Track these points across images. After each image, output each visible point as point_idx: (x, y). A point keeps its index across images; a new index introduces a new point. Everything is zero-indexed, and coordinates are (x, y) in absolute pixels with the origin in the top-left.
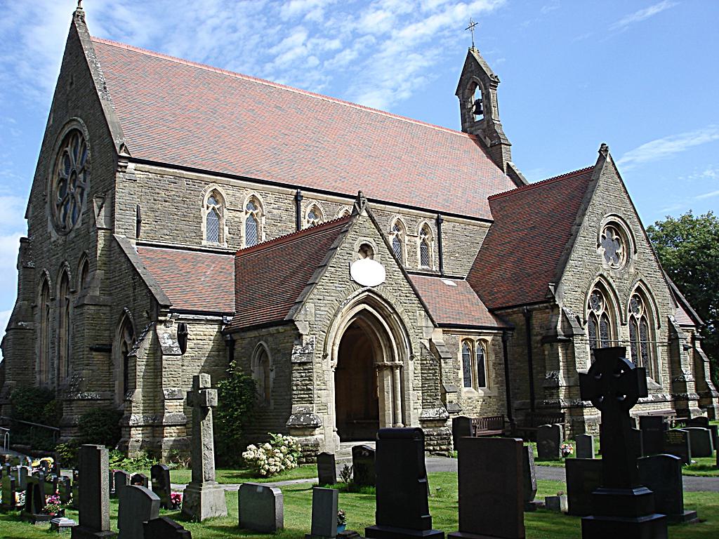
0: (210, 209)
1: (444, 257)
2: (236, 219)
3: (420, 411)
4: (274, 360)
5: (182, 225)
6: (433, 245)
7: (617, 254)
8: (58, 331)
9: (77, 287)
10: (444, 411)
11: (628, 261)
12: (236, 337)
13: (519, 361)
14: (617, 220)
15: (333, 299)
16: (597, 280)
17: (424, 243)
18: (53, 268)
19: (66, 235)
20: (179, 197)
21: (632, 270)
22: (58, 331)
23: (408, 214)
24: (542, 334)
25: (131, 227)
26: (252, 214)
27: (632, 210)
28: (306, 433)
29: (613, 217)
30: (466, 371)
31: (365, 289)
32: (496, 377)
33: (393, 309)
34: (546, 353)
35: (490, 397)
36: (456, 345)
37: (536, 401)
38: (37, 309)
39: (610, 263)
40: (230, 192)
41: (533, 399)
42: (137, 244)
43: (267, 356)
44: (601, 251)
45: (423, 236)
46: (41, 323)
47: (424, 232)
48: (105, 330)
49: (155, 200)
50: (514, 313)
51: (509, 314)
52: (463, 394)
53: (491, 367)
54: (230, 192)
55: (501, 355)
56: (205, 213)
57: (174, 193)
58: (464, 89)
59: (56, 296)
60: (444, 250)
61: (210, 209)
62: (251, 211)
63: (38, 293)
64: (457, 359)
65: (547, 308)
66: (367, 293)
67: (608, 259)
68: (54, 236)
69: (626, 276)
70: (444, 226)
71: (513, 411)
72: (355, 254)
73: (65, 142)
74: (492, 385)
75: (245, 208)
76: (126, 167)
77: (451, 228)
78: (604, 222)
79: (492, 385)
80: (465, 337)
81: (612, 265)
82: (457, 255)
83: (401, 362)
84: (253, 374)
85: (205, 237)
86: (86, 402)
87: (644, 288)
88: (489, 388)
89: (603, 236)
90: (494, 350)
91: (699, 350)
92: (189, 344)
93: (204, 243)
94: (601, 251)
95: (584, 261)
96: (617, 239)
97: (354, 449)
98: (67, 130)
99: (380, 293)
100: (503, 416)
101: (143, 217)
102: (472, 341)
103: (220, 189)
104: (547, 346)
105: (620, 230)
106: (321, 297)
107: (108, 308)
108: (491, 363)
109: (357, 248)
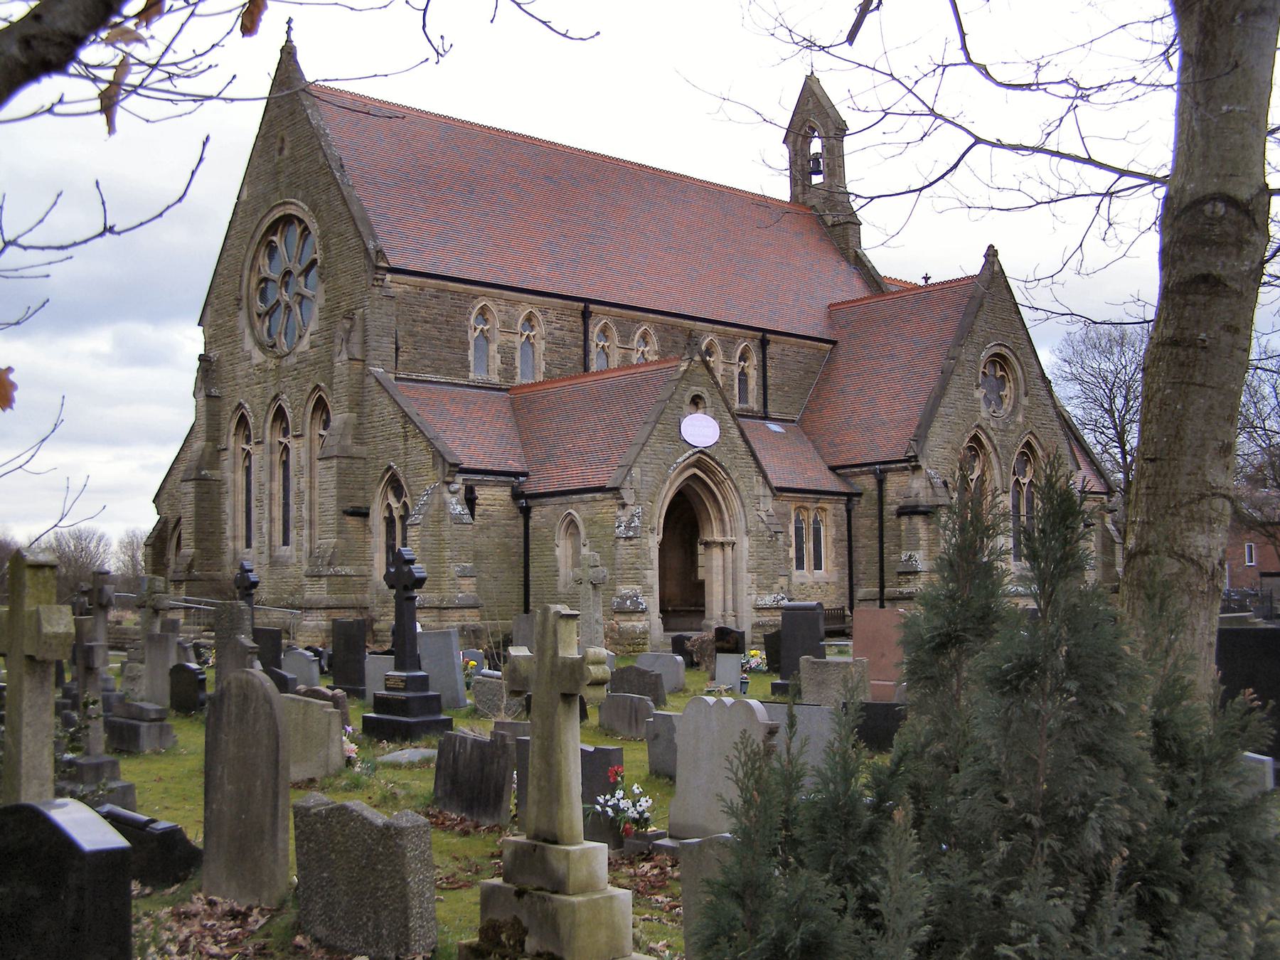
0: (478, 331)
1: (769, 392)
2: (510, 344)
3: (754, 597)
4: (588, 534)
5: (445, 353)
6: (753, 375)
7: (1000, 397)
8: (267, 485)
9: (303, 429)
10: (783, 598)
11: (1014, 407)
12: (531, 503)
13: (867, 537)
14: (1004, 351)
15: (661, 462)
16: (973, 433)
17: (743, 375)
18: (256, 401)
19: (280, 357)
20: (442, 315)
21: (1020, 419)
22: (267, 485)
23: (725, 334)
24: (898, 503)
25: (389, 358)
26: (528, 337)
27: (1025, 337)
28: (633, 618)
29: (998, 348)
30: (799, 550)
31: (697, 450)
32: (836, 557)
33: (728, 474)
34: (903, 527)
35: (827, 583)
36: (787, 515)
37: (886, 590)
38: (227, 453)
39: (991, 410)
40: (503, 308)
41: (882, 587)
42: (397, 379)
43: (577, 527)
44: (979, 394)
45: (742, 363)
46: (234, 472)
47: (743, 358)
48: (360, 489)
49: (414, 321)
50: (863, 473)
51: (856, 474)
52: (794, 579)
53: (830, 545)
54: (503, 308)
55: (844, 529)
56: (472, 335)
57: (436, 311)
58: (797, 134)
59: (264, 438)
60: (770, 381)
61: (478, 331)
62: (527, 333)
63: (229, 431)
64: (788, 532)
65: (906, 469)
66: (698, 455)
67: (988, 403)
68: (258, 357)
69: (1011, 427)
70: (772, 349)
71: (856, 601)
72: (686, 408)
73: (273, 229)
74: (830, 568)
75: (519, 328)
76: (383, 280)
77: (779, 352)
78: (984, 355)
79: (830, 568)
80: (799, 504)
81: (994, 412)
82: (786, 389)
83: (734, 538)
84: (557, 549)
85: (472, 368)
86: (340, 579)
87: (1034, 442)
88: (826, 571)
89: (984, 373)
90: (835, 522)
91: (1111, 527)
92: (478, 510)
93: (471, 376)
94: (979, 394)
95: (957, 408)
96: (1002, 376)
97: (427, 690)
98: (277, 214)
99: (712, 455)
100: (843, 609)
101: (400, 343)
102: (807, 509)
103: (490, 304)
104: (905, 520)
105: (1007, 364)
106: (648, 461)
107: (363, 462)
108: (830, 540)
109: (687, 400)
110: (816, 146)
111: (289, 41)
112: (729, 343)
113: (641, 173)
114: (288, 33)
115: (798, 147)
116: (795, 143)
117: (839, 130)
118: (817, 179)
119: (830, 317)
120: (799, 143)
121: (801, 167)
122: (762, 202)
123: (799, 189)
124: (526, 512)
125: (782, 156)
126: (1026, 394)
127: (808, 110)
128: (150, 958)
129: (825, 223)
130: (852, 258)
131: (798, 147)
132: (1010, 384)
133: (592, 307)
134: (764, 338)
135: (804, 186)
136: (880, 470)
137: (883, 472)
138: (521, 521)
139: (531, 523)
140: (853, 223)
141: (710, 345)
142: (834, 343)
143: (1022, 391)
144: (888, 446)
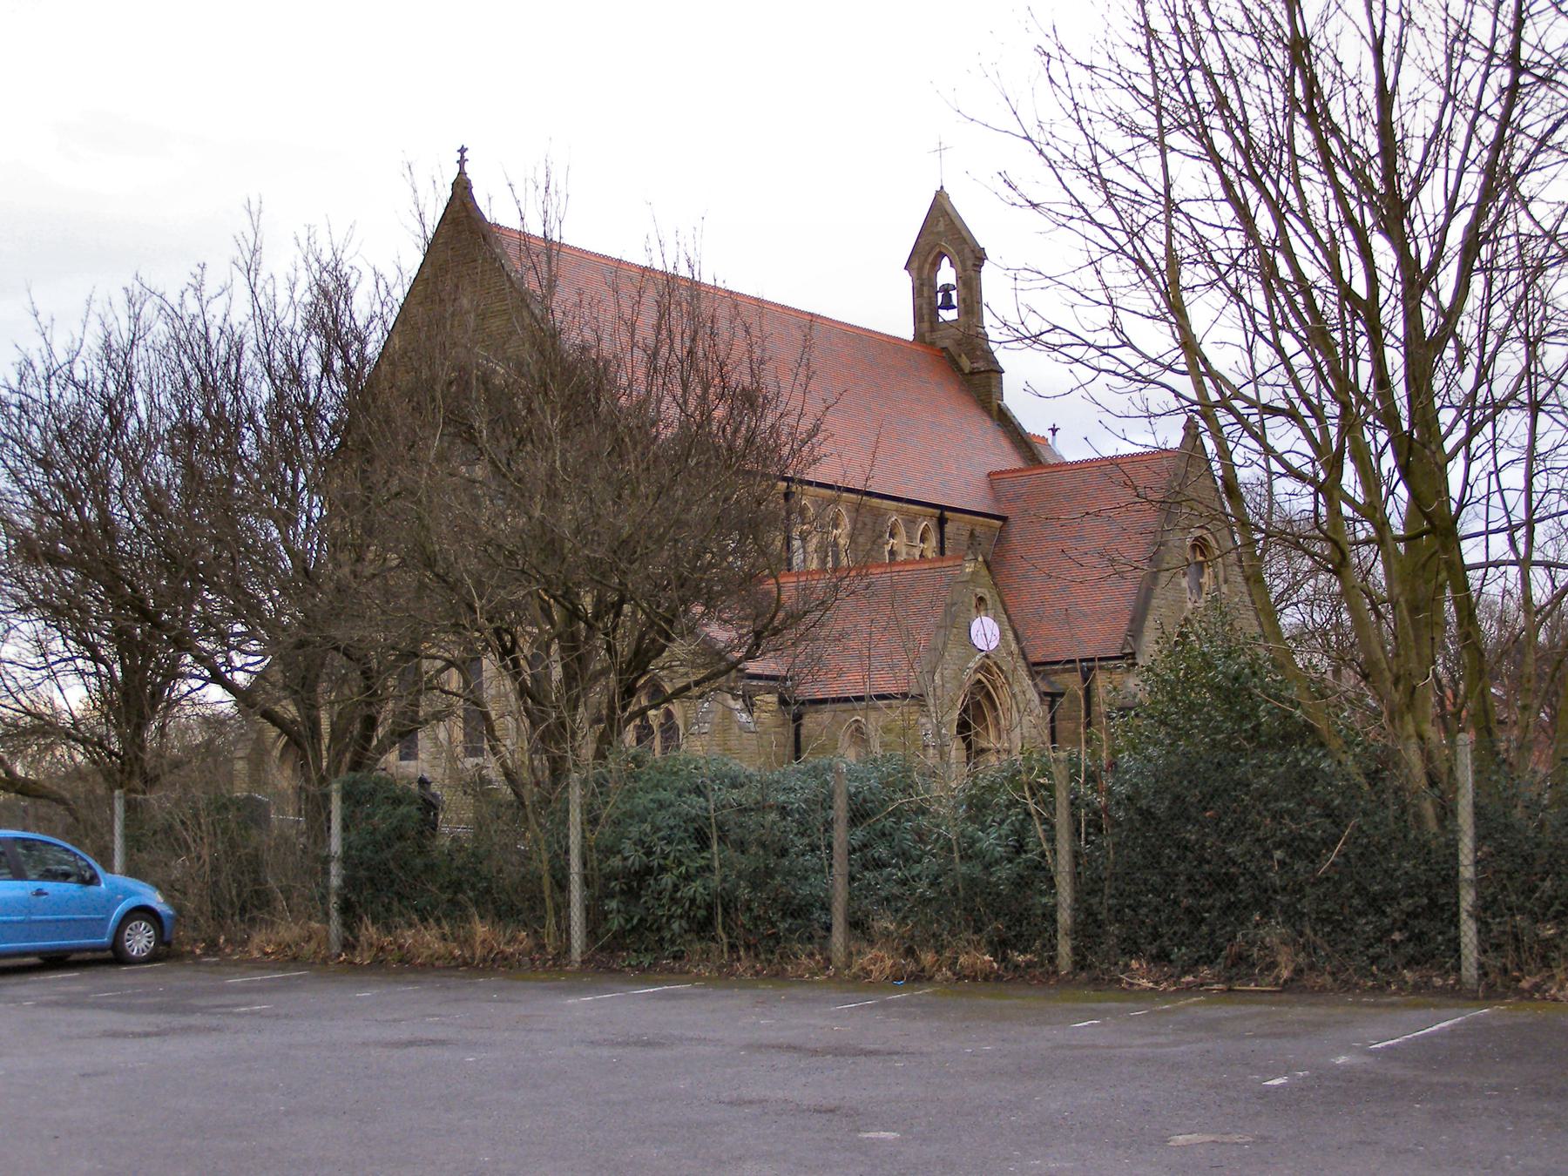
23: (907, 512)
50: (1065, 671)
51: (1056, 672)
58: (922, 261)
70: (949, 528)
110: (947, 274)
111: (462, 173)
112: (911, 521)
113: (784, 316)
114: (462, 162)
115: (925, 276)
116: (920, 269)
117: (972, 258)
118: (949, 315)
119: (992, 488)
120: (926, 271)
121: (926, 300)
122: (895, 342)
123: (926, 325)
124: (798, 718)
125: (903, 286)
126: (1226, 581)
127: (938, 233)
128: (1565, 841)
129: (961, 370)
130: (995, 413)
131: (925, 276)
132: (1208, 571)
133: (948, 514)
134: (942, 515)
135: (931, 323)
136: (1087, 668)
137: (1091, 669)
138: (792, 726)
139: (803, 731)
140: (995, 371)
141: (894, 525)
142: (1004, 519)
143: (1221, 579)
144: (1096, 638)
